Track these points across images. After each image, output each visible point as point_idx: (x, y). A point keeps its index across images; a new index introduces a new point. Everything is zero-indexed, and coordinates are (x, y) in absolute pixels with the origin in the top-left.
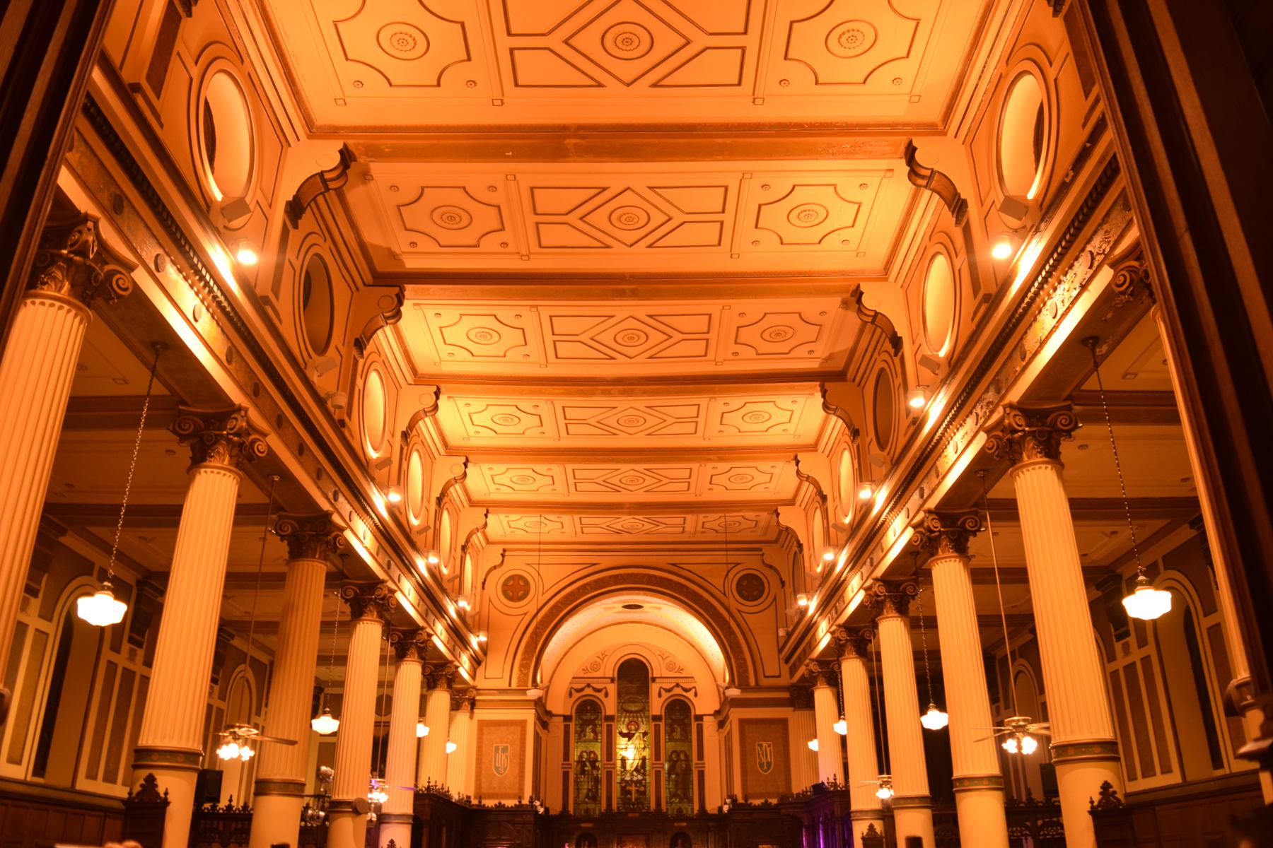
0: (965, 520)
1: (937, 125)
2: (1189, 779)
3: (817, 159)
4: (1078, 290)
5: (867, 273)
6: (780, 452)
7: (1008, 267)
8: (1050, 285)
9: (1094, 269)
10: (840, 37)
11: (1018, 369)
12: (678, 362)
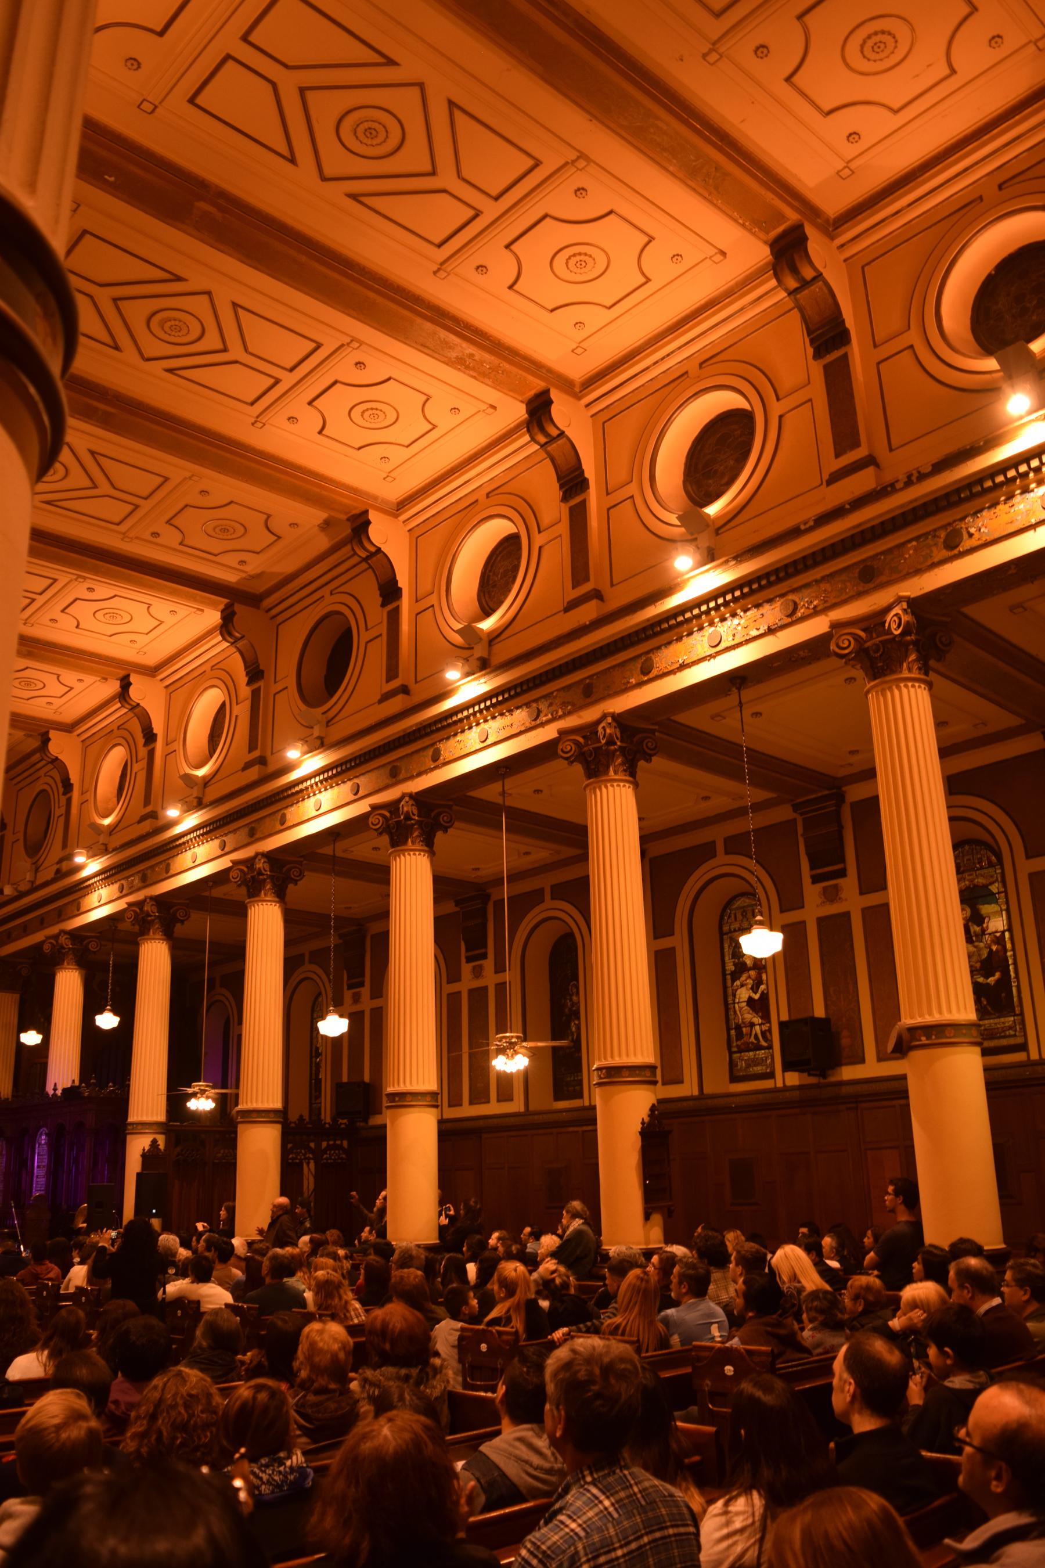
0: (439, 814)
1: (574, 386)
2: (531, 1108)
4: (762, 631)
5: (380, 500)
6: (110, 666)
7: (677, 578)
8: (719, 613)
9: (794, 618)
10: (570, 258)
11: (633, 681)
12: (60, 514)
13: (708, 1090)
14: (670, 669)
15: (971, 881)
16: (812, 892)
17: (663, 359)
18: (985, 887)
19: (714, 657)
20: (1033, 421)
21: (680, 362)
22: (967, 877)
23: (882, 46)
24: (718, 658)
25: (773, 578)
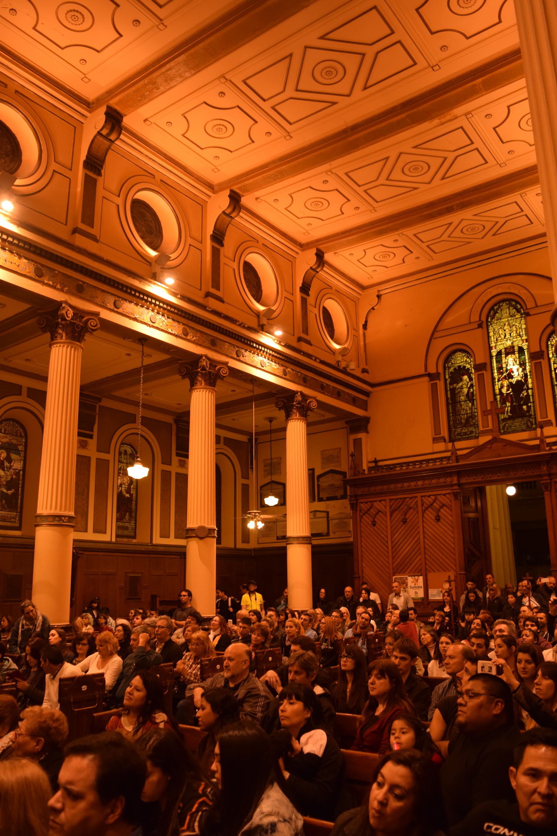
3: (258, 190)
4: (173, 332)
13: (238, 547)
14: (129, 315)
15: (10, 440)
16: (175, 459)
17: (151, 159)
18: (16, 445)
19: (150, 327)
20: (164, 288)
21: (154, 168)
22: (8, 437)
23: (221, 130)
24: (151, 328)
25: (125, 289)
